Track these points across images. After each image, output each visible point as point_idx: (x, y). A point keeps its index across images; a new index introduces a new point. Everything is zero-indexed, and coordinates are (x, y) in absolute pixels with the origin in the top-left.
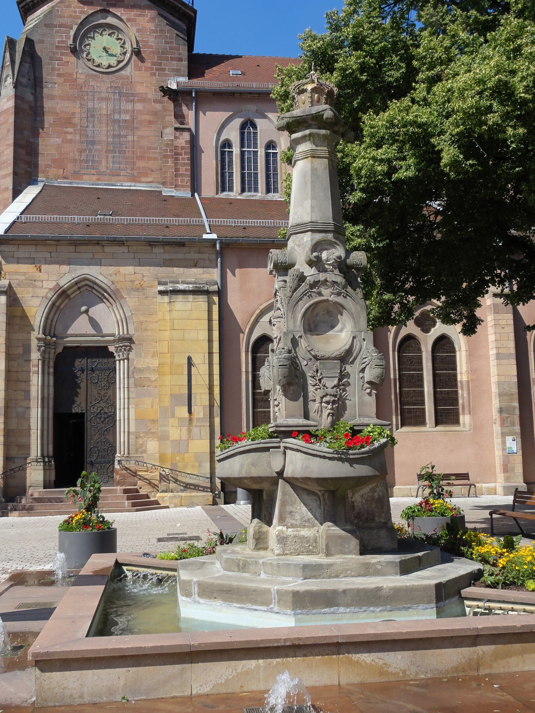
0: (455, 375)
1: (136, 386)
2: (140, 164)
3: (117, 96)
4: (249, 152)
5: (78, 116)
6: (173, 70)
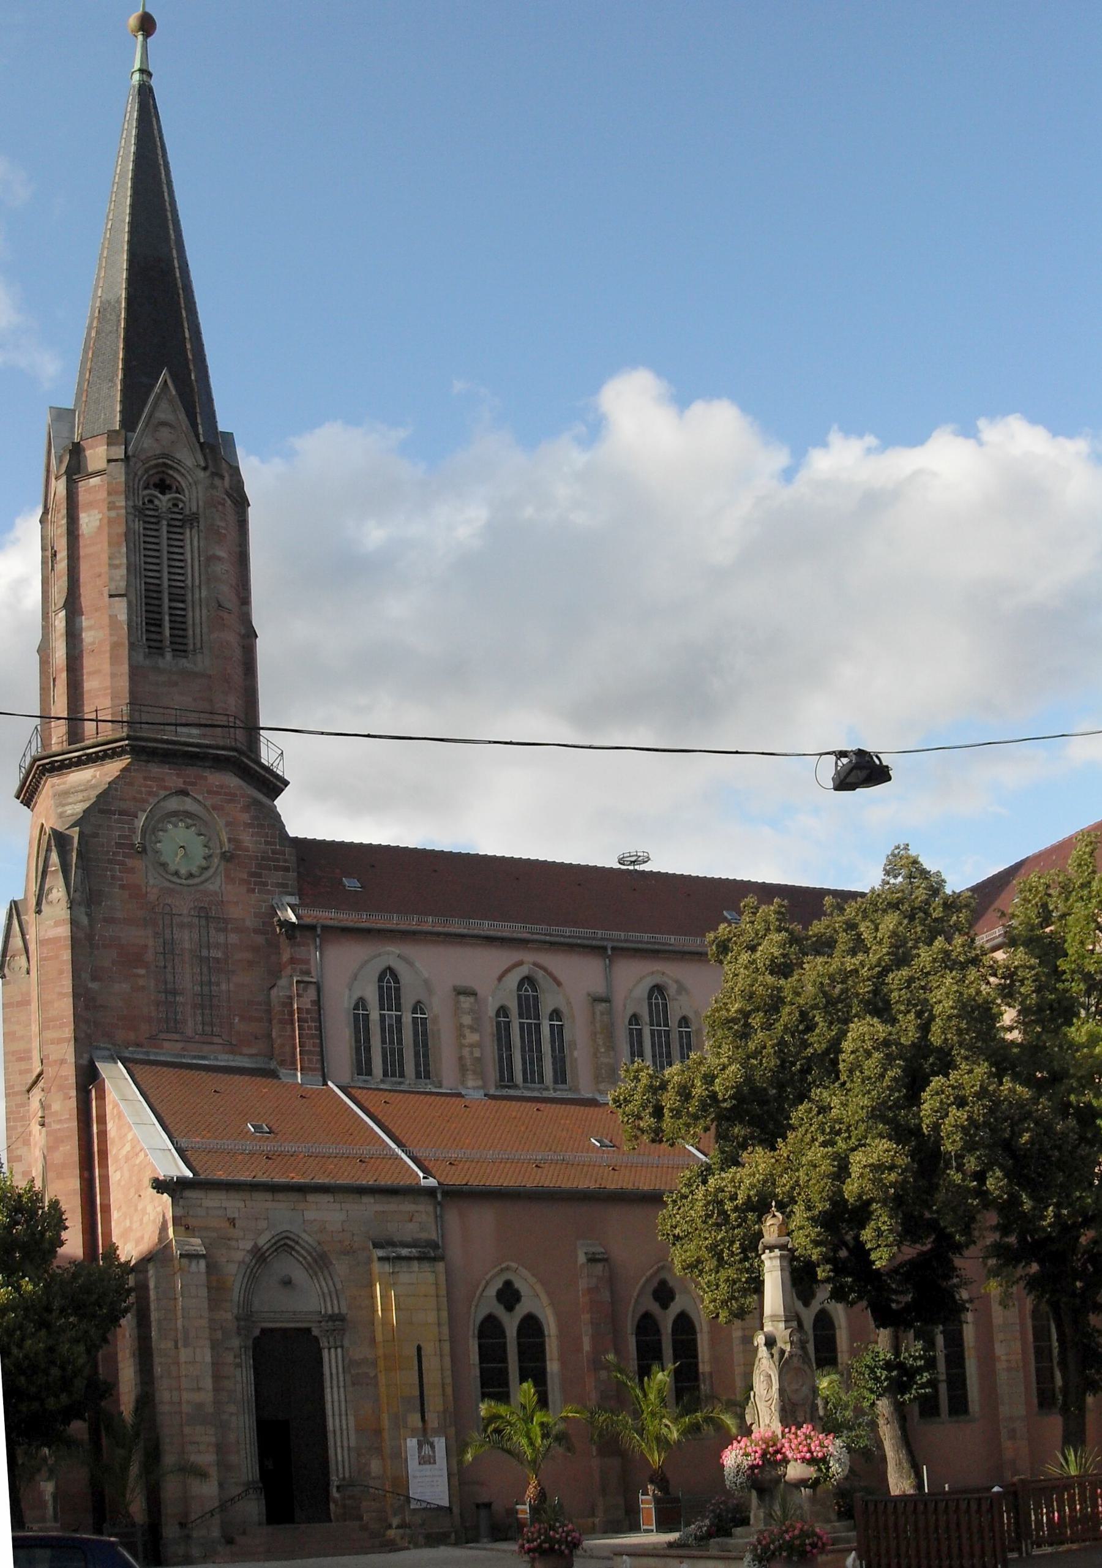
0: (696, 1365)
3: (203, 922)
4: (390, 1016)
6: (279, 885)
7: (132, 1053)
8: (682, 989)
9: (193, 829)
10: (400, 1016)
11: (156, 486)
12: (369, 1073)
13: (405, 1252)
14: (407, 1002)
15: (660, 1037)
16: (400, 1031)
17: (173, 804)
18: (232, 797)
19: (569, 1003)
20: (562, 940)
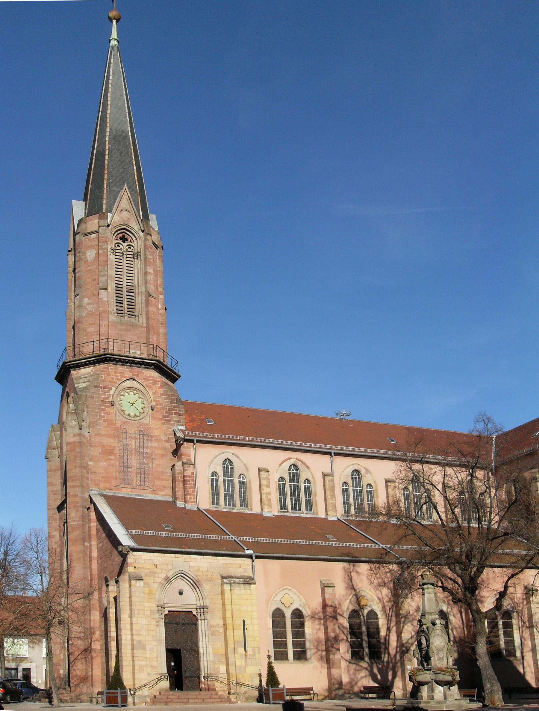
1: (212, 635)
2: (158, 483)
4: (228, 480)
5: (117, 448)
7: (107, 492)
8: (368, 471)
9: (137, 395)
10: (309, 487)
11: (121, 238)
12: (218, 504)
13: (237, 580)
14: (237, 473)
15: (357, 492)
16: (232, 487)
17: (128, 384)
18: (155, 382)
19: (313, 476)
20: (310, 449)
